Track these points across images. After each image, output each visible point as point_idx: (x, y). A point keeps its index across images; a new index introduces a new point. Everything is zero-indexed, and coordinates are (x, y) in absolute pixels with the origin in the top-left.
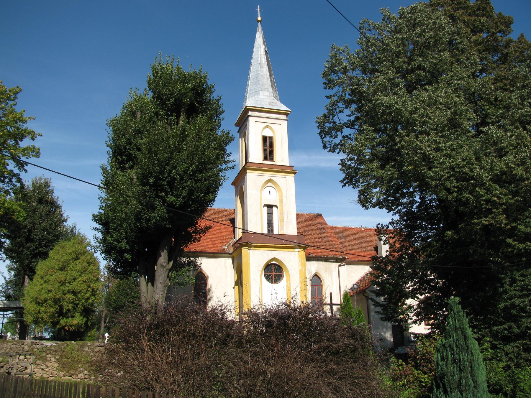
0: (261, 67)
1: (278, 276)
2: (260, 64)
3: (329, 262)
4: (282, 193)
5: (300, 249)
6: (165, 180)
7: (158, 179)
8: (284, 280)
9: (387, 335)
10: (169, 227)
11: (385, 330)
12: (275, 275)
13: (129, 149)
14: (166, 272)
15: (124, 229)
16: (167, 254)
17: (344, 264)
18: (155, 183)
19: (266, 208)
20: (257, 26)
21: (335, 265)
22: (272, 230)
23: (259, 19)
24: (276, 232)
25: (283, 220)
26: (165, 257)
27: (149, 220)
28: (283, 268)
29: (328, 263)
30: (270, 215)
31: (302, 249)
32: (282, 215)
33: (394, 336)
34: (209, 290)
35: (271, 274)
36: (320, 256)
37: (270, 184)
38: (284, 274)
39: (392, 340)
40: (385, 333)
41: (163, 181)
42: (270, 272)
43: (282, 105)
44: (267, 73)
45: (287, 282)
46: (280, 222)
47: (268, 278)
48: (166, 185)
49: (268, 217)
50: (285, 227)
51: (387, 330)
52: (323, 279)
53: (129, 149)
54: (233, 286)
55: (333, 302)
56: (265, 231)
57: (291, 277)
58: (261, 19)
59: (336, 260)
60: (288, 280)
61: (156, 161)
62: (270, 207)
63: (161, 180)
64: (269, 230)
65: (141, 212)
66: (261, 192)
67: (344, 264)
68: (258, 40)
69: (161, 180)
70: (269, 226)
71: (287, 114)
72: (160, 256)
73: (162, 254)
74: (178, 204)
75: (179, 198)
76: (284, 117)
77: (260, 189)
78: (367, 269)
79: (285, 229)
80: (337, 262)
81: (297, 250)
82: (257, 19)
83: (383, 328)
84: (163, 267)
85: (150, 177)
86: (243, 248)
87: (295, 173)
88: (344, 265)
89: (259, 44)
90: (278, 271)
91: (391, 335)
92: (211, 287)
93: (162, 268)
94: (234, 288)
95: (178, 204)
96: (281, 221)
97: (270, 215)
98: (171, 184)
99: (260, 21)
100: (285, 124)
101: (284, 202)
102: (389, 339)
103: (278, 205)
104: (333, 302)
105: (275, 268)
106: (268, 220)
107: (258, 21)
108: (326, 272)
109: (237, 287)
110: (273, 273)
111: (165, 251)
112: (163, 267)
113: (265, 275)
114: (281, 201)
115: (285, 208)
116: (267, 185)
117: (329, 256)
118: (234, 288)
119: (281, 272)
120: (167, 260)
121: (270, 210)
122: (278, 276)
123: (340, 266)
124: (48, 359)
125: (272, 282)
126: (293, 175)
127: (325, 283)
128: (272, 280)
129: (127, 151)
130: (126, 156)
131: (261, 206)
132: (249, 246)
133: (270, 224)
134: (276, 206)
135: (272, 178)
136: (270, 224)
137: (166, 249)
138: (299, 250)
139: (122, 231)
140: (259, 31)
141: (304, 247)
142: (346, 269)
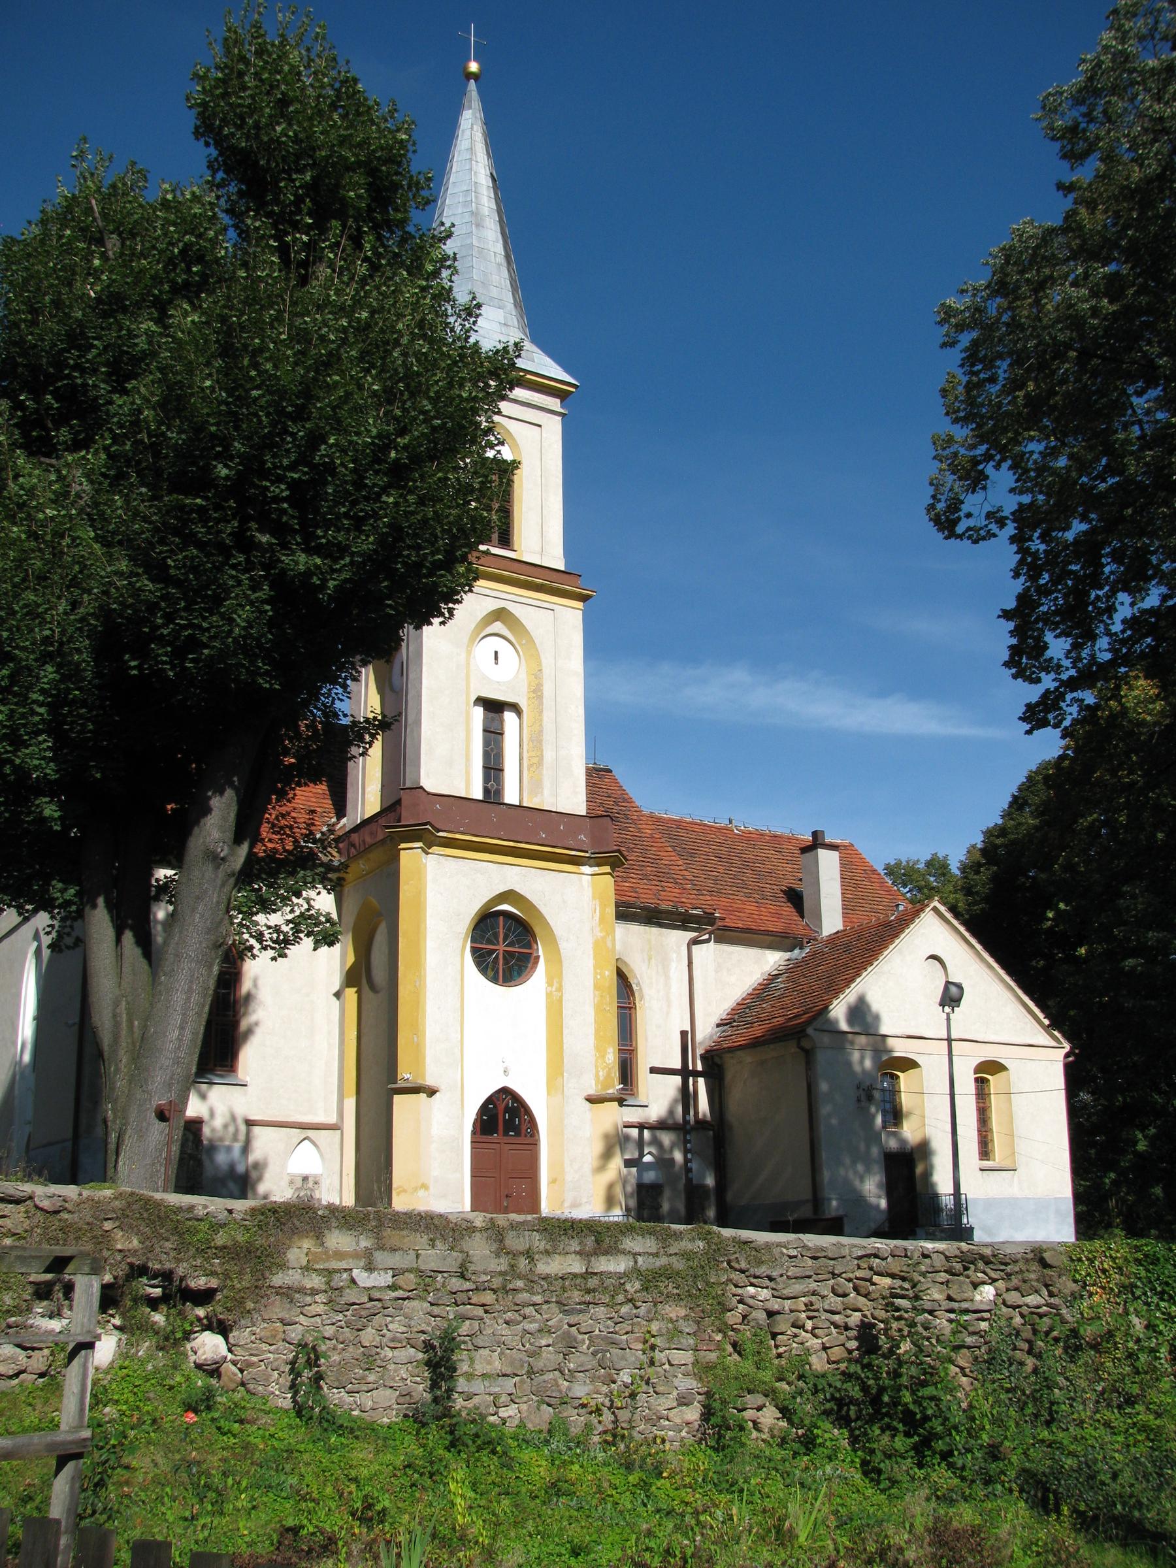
0: (478, 225)
1: (518, 960)
2: (475, 214)
3: (661, 925)
4: (540, 664)
5: (598, 865)
6: (280, 479)
7: (253, 468)
8: (539, 977)
9: (867, 1187)
10: (272, 690)
11: (860, 1168)
12: (509, 955)
13: (77, 367)
14: (223, 885)
15: (43, 692)
16: (234, 809)
17: (706, 937)
18: (238, 486)
19: (479, 712)
20: (463, 92)
21: (677, 939)
22: (499, 792)
23: (474, 67)
24: (511, 796)
25: (541, 757)
26: (224, 819)
27: (194, 644)
28: (537, 930)
29: (655, 931)
30: (493, 736)
31: (607, 869)
32: (534, 744)
33: (889, 1188)
34: (249, 997)
35: (494, 951)
36: (633, 905)
37: (498, 627)
38: (541, 953)
39: (883, 1203)
40: (862, 1180)
41: (272, 483)
42: (489, 942)
43: (548, 361)
44: (499, 248)
45: (550, 983)
46: (530, 766)
47: (482, 960)
48: (284, 500)
49: (486, 743)
50: (547, 783)
51: (868, 1170)
52: (638, 984)
53: (77, 367)
54: (336, 987)
55: (677, 1065)
56: (478, 794)
57: (565, 964)
58: (481, 70)
59: (679, 920)
60: (555, 978)
61: (258, 388)
62: (494, 707)
63: (264, 474)
64: (487, 791)
65: (153, 607)
66: (469, 652)
67: (706, 937)
68: (468, 133)
69: (264, 474)
70: (487, 779)
71: (562, 395)
72: (207, 811)
73: (216, 802)
74: (331, 584)
75: (336, 560)
76: (554, 403)
77: (466, 640)
78: (772, 960)
79: (546, 792)
80: (685, 929)
81: (586, 869)
82: (465, 68)
83: (854, 1163)
84: (216, 860)
85: (218, 456)
86: (403, 846)
87: (584, 598)
88: (707, 941)
89: (471, 149)
90: (519, 941)
91: (879, 1186)
92: (255, 985)
93: (210, 867)
94: (338, 995)
95: (331, 584)
96: (533, 762)
97: (493, 736)
98: (304, 497)
99: (476, 77)
100: (553, 427)
101: (545, 694)
102: (873, 1200)
103: (523, 705)
104: (677, 1065)
105: (509, 929)
106: (486, 755)
107: (469, 76)
108: (650, 959)
109: (351, 994)
110: (501, 947)
111: (229, 793)
112: (216, 860)
113: (474, 950)
114: (537, 692)
115: (548, 716)
116: (489, 630)
117: (663, 906)
118: (338, 995)
119: (530, 947)
120: (230, 835)
121: (493, 720)
122: (518, 960)
123: (694, 942)
124: (819, 1441)
125: (494, 980)
126: (580, 605)
127: (647, 998)
128: (497, 972)
129: (68, 377)
130: (57, 396)
131: (468, 704)
132: (427, 836)
133: (493, 769)
134: (515, 708)
135: (511, 607)
136: (493, 769)
137: (232, 785)
138: (596, 869)
139: (35, 696)
140: (470, 108)
141: (614, 861)
142: (709, 953)
